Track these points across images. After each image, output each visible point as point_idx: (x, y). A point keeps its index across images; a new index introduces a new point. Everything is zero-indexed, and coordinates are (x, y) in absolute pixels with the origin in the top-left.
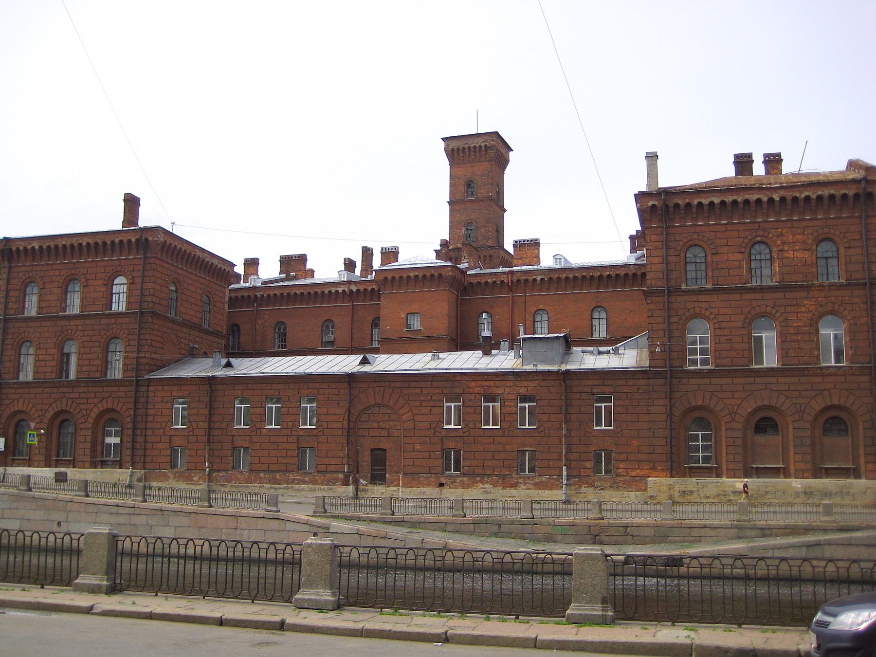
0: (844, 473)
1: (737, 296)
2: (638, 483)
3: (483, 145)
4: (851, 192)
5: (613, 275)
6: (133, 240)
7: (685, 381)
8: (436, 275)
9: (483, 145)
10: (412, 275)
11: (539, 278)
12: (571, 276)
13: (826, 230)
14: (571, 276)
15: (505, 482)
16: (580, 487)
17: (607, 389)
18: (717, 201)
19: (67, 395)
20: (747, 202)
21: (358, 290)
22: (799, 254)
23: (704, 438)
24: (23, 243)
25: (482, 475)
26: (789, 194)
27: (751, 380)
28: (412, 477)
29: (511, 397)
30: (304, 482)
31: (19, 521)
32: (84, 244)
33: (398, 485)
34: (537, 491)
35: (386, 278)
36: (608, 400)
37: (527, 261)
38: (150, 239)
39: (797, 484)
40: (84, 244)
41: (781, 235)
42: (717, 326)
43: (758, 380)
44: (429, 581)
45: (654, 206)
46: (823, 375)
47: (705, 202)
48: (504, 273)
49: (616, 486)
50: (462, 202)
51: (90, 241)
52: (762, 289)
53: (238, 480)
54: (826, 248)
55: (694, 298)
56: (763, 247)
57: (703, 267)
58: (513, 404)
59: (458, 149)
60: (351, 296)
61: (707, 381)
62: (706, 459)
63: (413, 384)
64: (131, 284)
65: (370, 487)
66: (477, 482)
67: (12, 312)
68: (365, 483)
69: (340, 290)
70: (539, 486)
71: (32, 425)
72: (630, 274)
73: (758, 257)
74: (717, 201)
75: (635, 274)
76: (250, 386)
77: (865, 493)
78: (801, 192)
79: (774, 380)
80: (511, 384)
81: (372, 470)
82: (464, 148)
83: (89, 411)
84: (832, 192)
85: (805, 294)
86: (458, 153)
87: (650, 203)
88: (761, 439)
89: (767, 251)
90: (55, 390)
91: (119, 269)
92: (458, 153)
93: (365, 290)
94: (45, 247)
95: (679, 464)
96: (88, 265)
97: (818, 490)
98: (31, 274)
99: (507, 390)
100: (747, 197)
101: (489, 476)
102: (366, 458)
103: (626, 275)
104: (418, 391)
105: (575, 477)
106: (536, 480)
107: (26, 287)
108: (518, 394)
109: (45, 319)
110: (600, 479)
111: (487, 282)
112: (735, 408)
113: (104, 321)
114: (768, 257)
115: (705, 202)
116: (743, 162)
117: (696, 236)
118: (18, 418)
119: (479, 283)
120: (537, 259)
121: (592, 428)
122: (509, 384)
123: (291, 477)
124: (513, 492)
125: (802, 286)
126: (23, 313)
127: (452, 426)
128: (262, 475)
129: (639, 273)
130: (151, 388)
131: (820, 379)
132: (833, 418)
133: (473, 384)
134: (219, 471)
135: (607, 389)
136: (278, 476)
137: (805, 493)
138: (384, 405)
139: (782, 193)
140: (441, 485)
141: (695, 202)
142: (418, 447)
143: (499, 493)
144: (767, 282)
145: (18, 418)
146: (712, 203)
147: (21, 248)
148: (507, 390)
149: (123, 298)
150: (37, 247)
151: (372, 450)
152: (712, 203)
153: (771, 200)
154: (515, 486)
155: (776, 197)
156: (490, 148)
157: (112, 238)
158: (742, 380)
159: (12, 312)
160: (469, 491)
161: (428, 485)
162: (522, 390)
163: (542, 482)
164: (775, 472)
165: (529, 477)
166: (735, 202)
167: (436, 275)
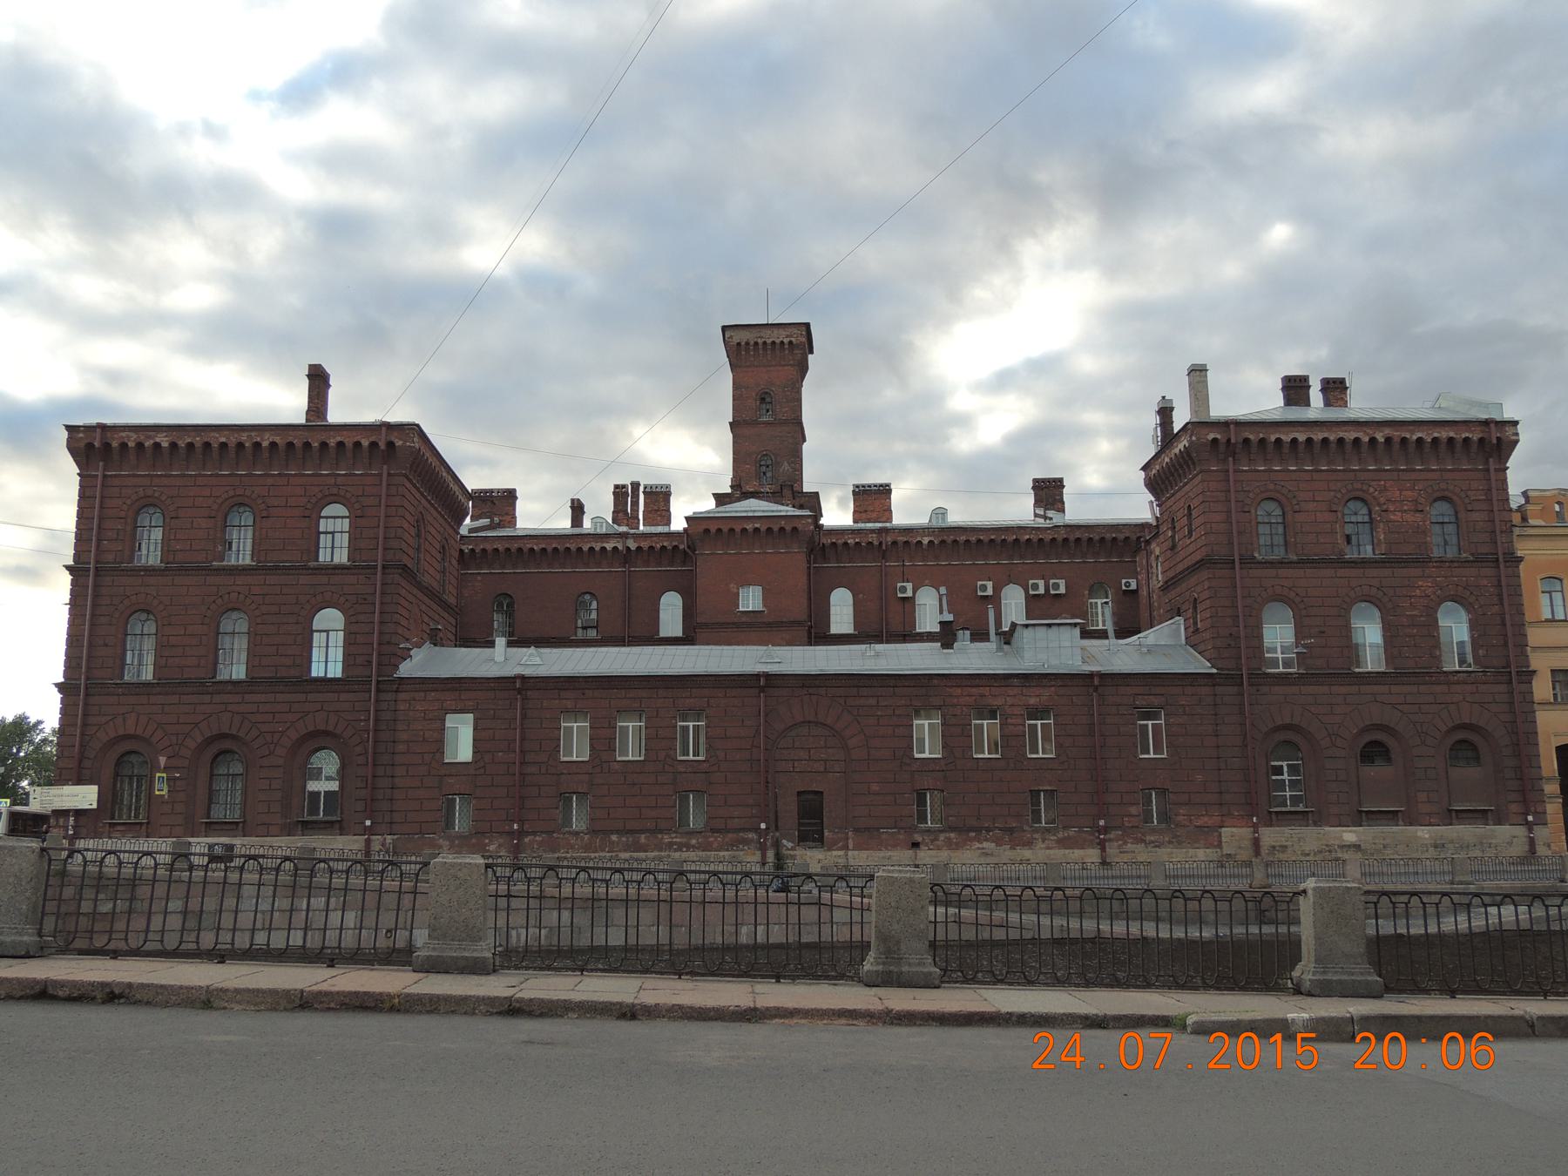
0: (1480, 816)
1: (1329, 572)
2: (1207, 834)
3: (786, 341)
4: (1475, 436)
5: (1035, 540)
6: (365, 443)
7: (1265, 689)
8: (788, 528)
9: (786, 341)
10: (749, 527)
11: (926, 541)
12: (973, 539)
13: (1443, 485)
14: (973, 539)
15: (1013, 836)
16: (1125, 843)
17: (1156, 701)
18: (1302, 438)
19: (230, 708)
20: (1341, 441)
21: (639, 548)
22: (1409, 517)
23: (1293, 770)
24: (134, 436)
25: (978, 830)
26: (1397, 434)
27: (1354, 689)
28: (869, 835)
29: (1017, 711)
30: (689, 847)
31: (202, 934)
32: (265, 444)
33: (846, 848)
34: (1062, 851)
35: (707, 531)
36: (1155, 716)
37: (874, 515)
38: (399, 443)
39: (1424, 833)
40: (265, 444)
41: (1386, 489)
42: (353, 619)
43: (1364, 689)
44: (772, 994)
45: (1215, 440)
46: (1448, 683)
47: (1287, 438)
48: (872, 531)
49: (1177, 842)
50: (747, 423)
51: (277, 439)
52: (1363, 563)
53: (572, 847)
54: (1441, 510)
55: (1272, 572)
56: (1359, 504)
57: (1280, 529)
58: (1019, 721)
59: (747, 343)
60: (626, 557)
61: (1295, 689)
62: (1295, 800)
63: (864, 691)
64: (355, 518)
65: (799, 852)
66: (971, 840)
67: (110, 557)
68: (790, 845)
69: (609, 546)
70: (1064, 843)
71: (162, 760)
72: (1060, 539)
73: (1353, 519)
74: (1302, 438)
75: (1066, 540)
76: (589, 693)
77: (1510, 844)
78: (1412, 432)
79: (1385, 689)
80: (1016, 691)
81: (800, 824)
82: (756, 343)
83: (277, 736)
84: (1452, 434)
85: (1418, 572)
86: (747, 350)
87: (1211, 436)
88: (1372, 771)
89: (1365, 511)
90: (207, 698)
91: (335, 491)
92: (747, 350)
93: (651, 548)
94: (181, 444)
95: (1261, 808)
96: (270, 481)
97: (1452, 842)
98: (149, 492)
99: (1010, 701)
100: (1341, 435)
101: (988, 830)
102: (789, 808)
103: (1054, 540)
104: (872, 701)
105: (1116, 828)
106: (1060, 835)
107: (138, 513)
108: (1027, 707)
109: (183, 570)
110: (1154, 831)
111: (846, 544)
112: (277, 736)
113: (303, 580)
114: (1366, 519)
115: (1287, 438)
116: (1295, 389)
117: (1271, 486)
118: (227, 745)
119: (834, 544)
120: (887, 512)
121: (557, 759)
122: (1011, 691)
123: (667, 839)
124: (1027, 853)
125: (1417, 561)
126: (131, 561)
127: (926, 755)
128: (614, 838)
129: (1072, 538)
130: (402, 696)
131: (1444, 688)
132: (1287, 742)
133: (959, 691)
134: (534, 833)
135: (1156, 701)
136: (643, 839)
137: (1436, 846)
138: (817, 723)
139: (1388, 431)
140: (916, 845)
141: (1273, 438)
142: (875, 787)
143: (1006, 854)
144: (1368, 552)
145: (227, 745)
146: (1294, 440)
147: (131, 444)
148: (1010, 701)
149: (343, 540)
150: (165, 444)
151: (799, 793)
152: (1294, 440)
153: (1373, 440)
154: (1029, 844)
155: (1380, 437)
156: (798, 346)
157: (322, 437)
158: (1343, 690)
159: (110, 557)
160: (958, 853)
161: (894, 846)
162: (1032, 701)
163: (1069, 838)
164: (1392, 817)
165: (1048, 830)
166: (1325, 441)
167: (788, 528)
